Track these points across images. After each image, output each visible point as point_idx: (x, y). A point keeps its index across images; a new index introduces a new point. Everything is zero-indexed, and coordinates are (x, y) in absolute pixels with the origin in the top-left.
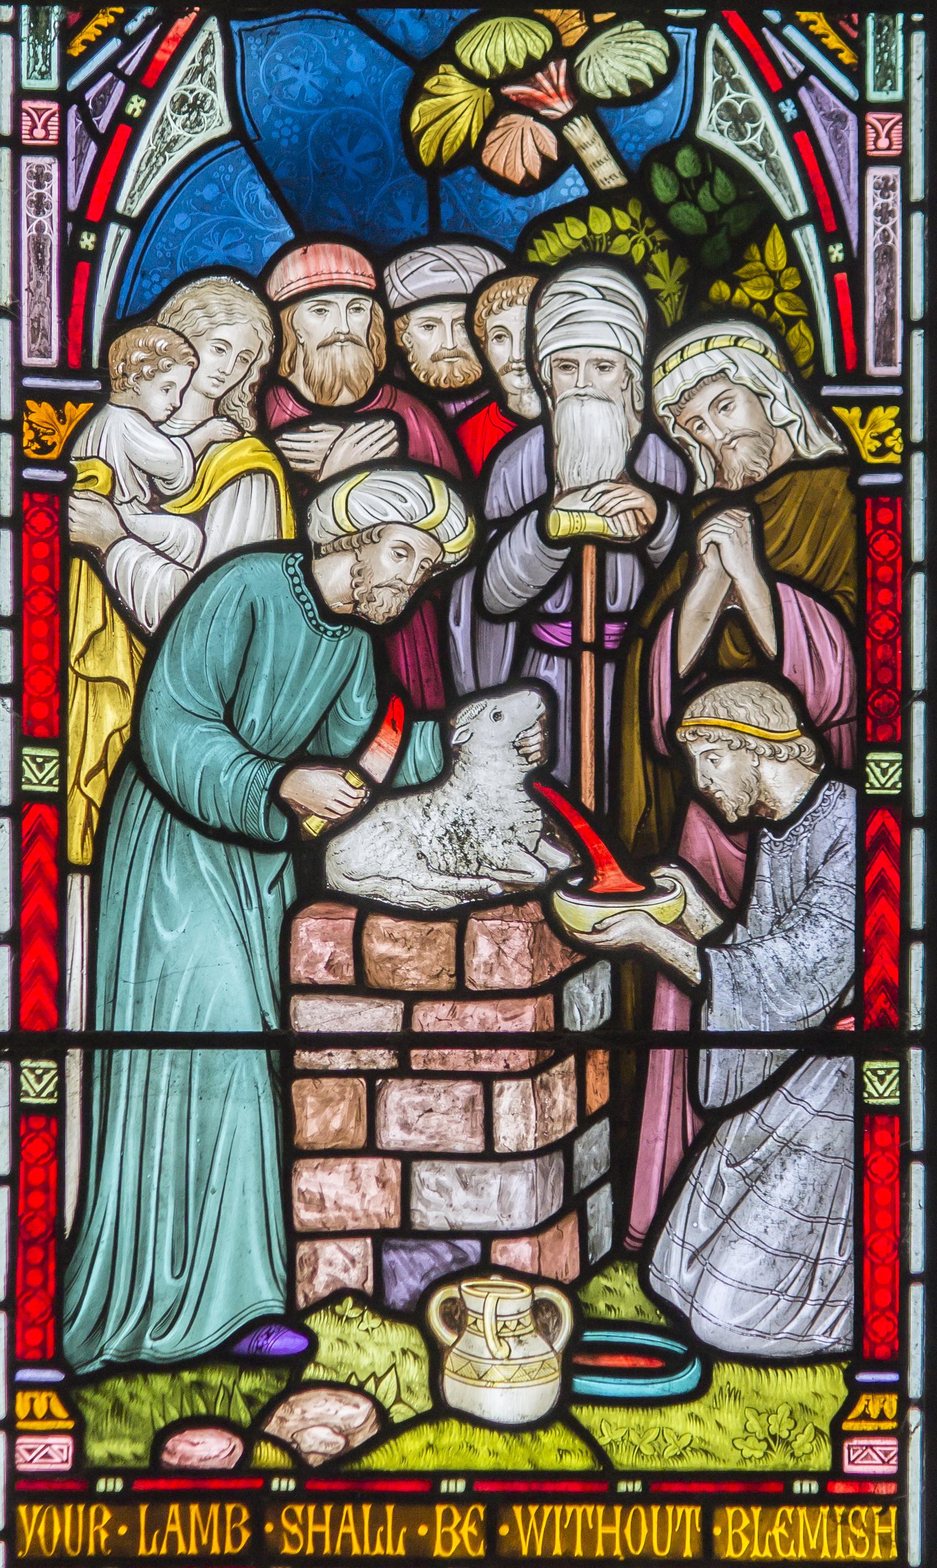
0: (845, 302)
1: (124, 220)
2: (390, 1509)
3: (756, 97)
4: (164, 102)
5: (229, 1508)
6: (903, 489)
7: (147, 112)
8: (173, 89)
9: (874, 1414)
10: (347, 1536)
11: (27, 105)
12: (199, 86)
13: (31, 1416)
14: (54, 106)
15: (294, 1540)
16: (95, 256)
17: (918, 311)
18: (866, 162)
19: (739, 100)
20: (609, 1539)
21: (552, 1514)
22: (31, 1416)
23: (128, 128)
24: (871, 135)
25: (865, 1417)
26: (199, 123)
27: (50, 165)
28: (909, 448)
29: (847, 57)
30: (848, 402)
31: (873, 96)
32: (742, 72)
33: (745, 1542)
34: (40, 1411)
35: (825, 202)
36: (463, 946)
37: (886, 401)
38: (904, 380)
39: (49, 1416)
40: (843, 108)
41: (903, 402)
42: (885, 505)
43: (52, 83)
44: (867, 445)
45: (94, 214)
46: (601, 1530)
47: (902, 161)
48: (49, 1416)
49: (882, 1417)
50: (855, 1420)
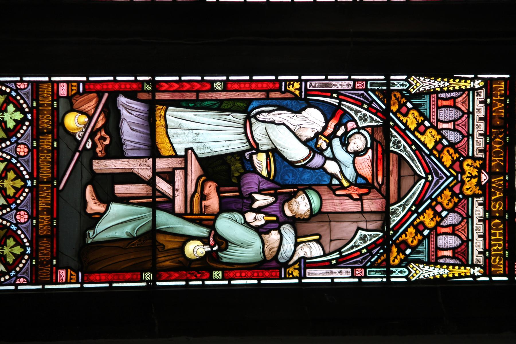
0: (323, 264)
2: (49, 207)
3: (368, 243)
4: (364, 112)
5: (50, 194)
6: (281, 278)
8: (368, 114)
11: (364, 82)
12: (369, 120)
13: (72, 86)
14: (364, 87)
15: (43, 117)
16: (331, 97)
19: (368, 239)
20: (43, 142)
22: (72, 86)
24: (359, 270)
25: (71, 275)
26: (361, 120)
27: (351, 87)
30: (300, 265)
31: (368, 270)
32: (374, 239)
33: (43, 158)
35: (345, 259)
36: (152, 217)
37: (300, 274)
39: (72, 90)
40: (364, 263)
42: (436, 205)
43: (369, 87)
44: (291, 270)
45: (341, 97)
46: (45, 141)
48: (72, 90)
50: (70, 273)
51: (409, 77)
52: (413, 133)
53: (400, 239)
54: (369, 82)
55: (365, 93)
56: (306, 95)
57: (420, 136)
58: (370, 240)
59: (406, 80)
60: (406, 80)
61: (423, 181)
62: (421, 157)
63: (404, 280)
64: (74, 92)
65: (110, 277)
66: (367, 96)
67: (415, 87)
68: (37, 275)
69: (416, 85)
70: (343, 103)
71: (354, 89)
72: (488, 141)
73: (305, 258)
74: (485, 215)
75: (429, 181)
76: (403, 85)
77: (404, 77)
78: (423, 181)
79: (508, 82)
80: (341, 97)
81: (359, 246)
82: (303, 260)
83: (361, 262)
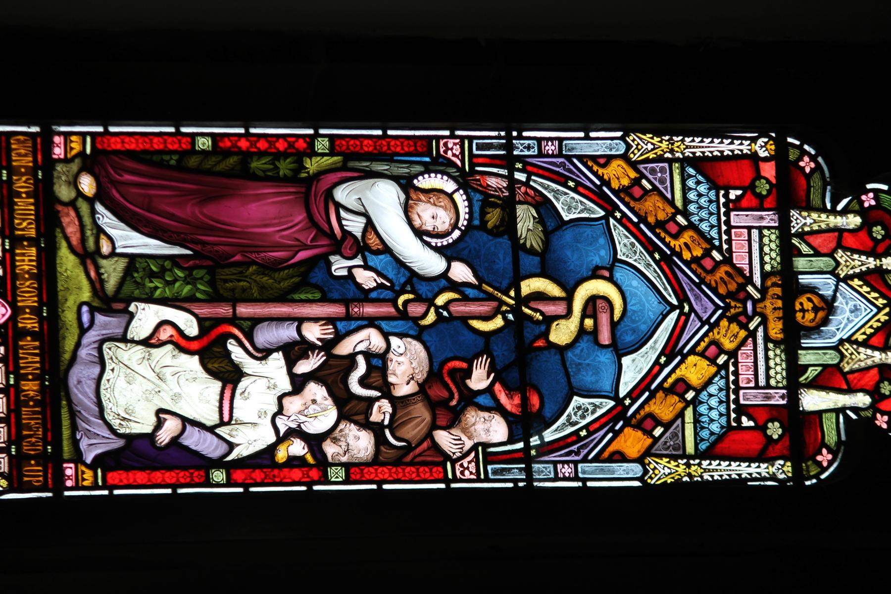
0: (505, 457)
1: (529, 179)
4: (572, 194)
5: (41, 479)
7: (569, 188)
9: (84, 476)
10: (27, 358)
13: (71, 141)
17: (589, 484)
18: (555, 463)
21: (39, 476)
22: (71, 141)
23: (562, 180)
28: (584, 480)
29: (606, 454)
34: (73, 145)
38: (487, 480)
41: (478, 480)
45: (529, 168)
47: (556, 479)
49: (84, 480)
51: (626, 134)
52: (651, 228)
53: (642, 413)
54: (475, 142)
55: (567, 163)
56: (472, 165)
57: (668, 239)
58: (593, 412)
59: (622, 138)
60: (622, 138)
61: (674, 315)
62: (670, 275)
63: (637, 484)
64: (74, 152)
65: (169, 476)
66: (572, 167)
67: (636, 151)
68: (21, 475)
69: (637, 148)
70: (533, 177)
71: (540, 155)
72: (7, 247)
73: (486, 445)
74: (7, 379)
75: (685, 314)
76: (529, 148)
77: (619, 134)
78: (674, 315)
79: (39, 140)
80: (529, 168)
81: (576, 423)
82: (480, 448)
83: (577, 453)
